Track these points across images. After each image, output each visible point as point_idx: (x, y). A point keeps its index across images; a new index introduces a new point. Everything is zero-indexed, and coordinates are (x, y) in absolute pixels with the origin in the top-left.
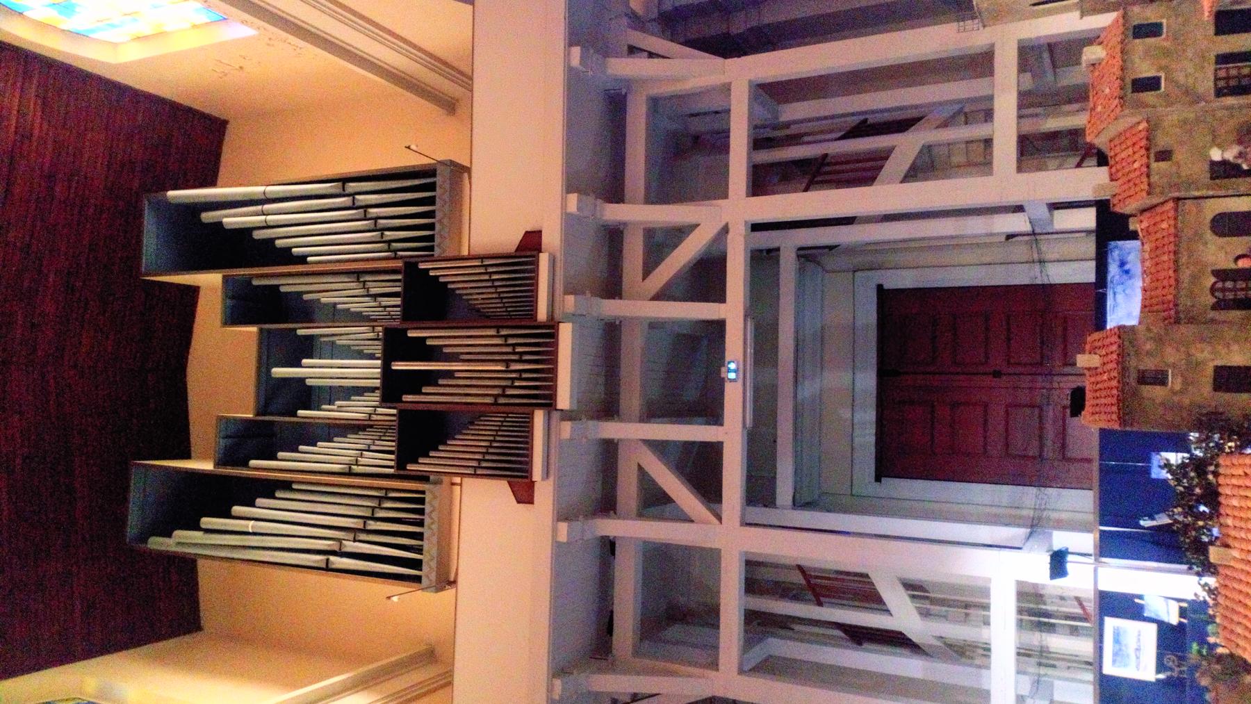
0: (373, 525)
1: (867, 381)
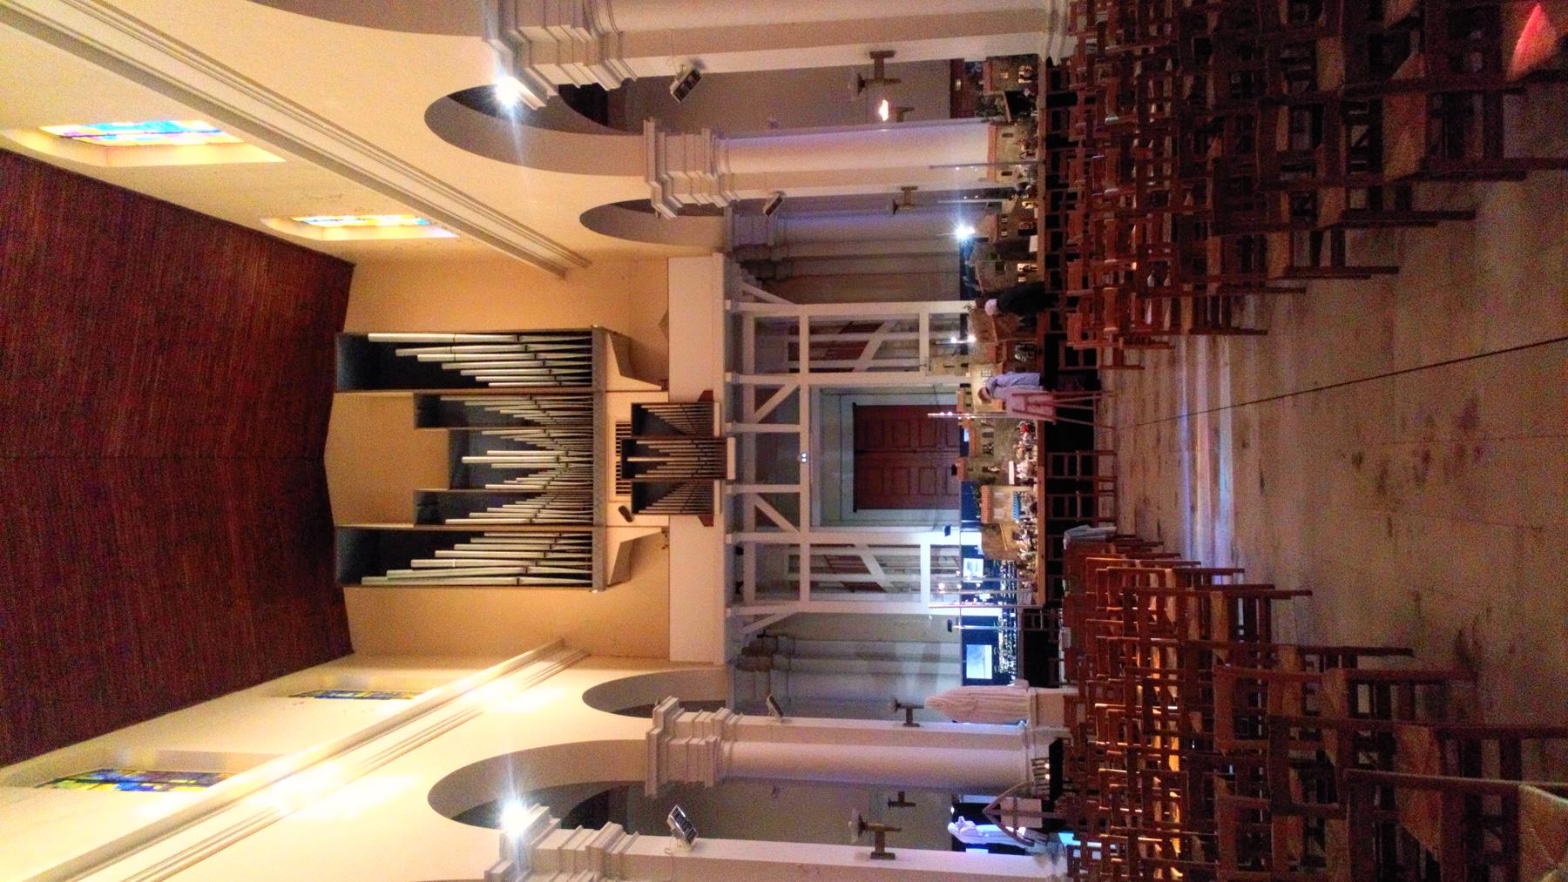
0: (551, 555)
1: (849, 457)
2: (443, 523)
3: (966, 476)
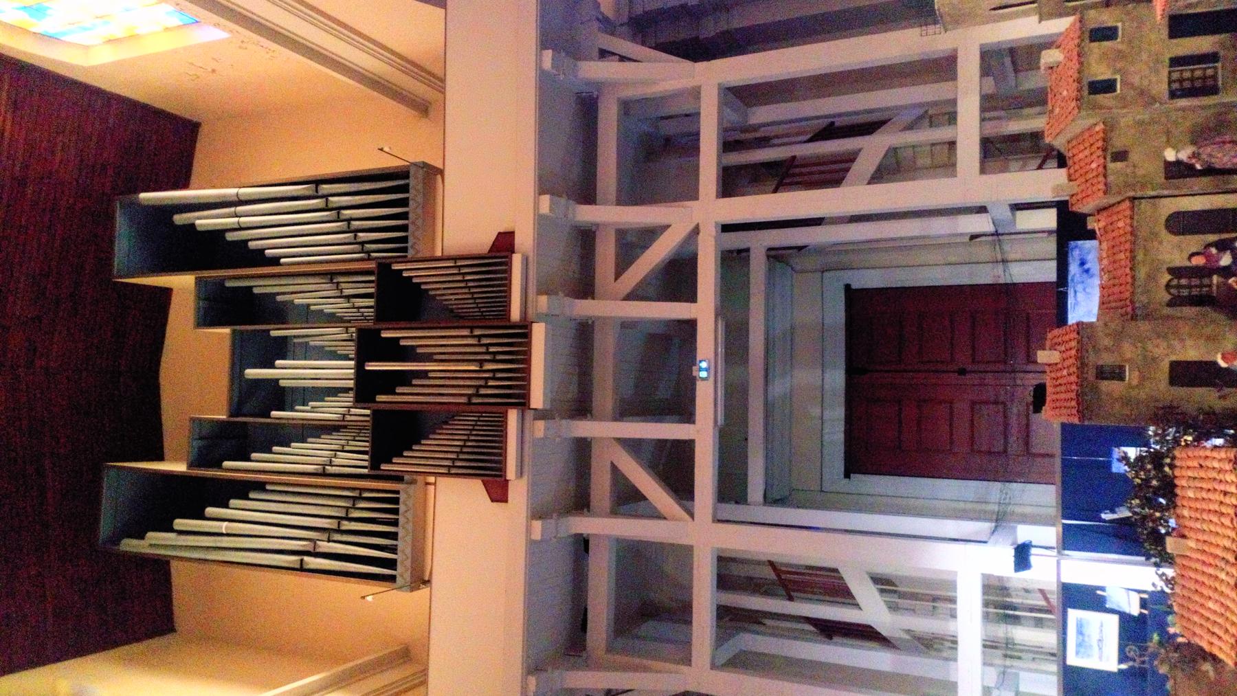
0: (347, 525)
1: (836, 378)
2: (219, 467)
3: (1085, 401)
